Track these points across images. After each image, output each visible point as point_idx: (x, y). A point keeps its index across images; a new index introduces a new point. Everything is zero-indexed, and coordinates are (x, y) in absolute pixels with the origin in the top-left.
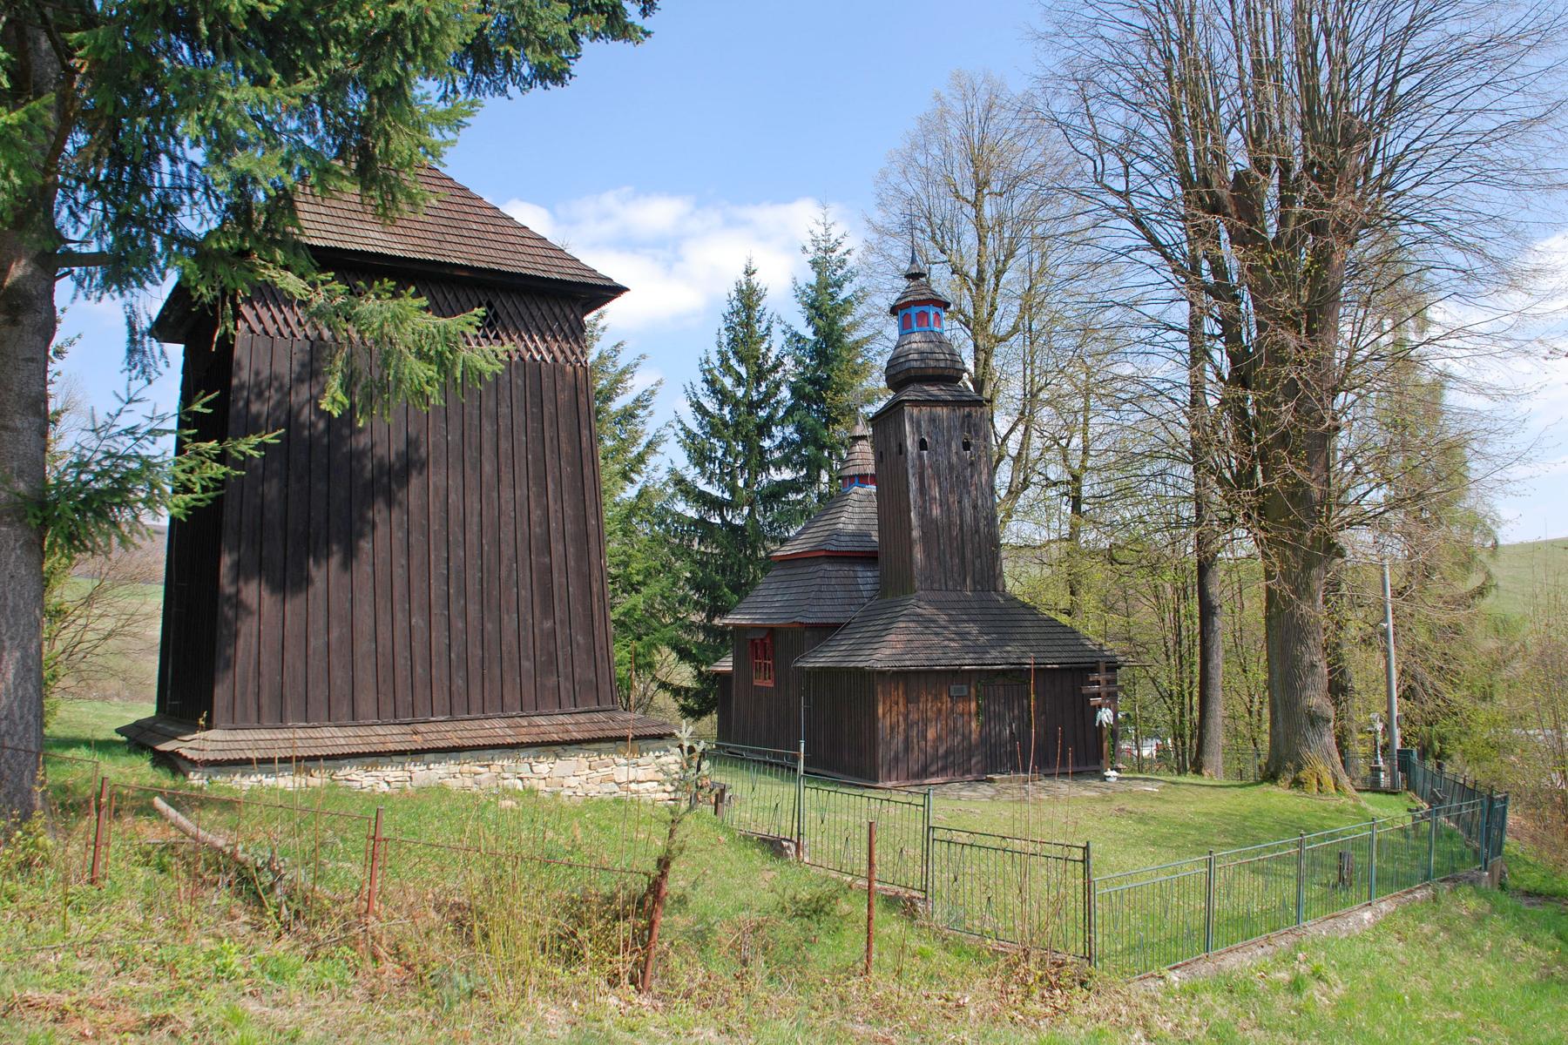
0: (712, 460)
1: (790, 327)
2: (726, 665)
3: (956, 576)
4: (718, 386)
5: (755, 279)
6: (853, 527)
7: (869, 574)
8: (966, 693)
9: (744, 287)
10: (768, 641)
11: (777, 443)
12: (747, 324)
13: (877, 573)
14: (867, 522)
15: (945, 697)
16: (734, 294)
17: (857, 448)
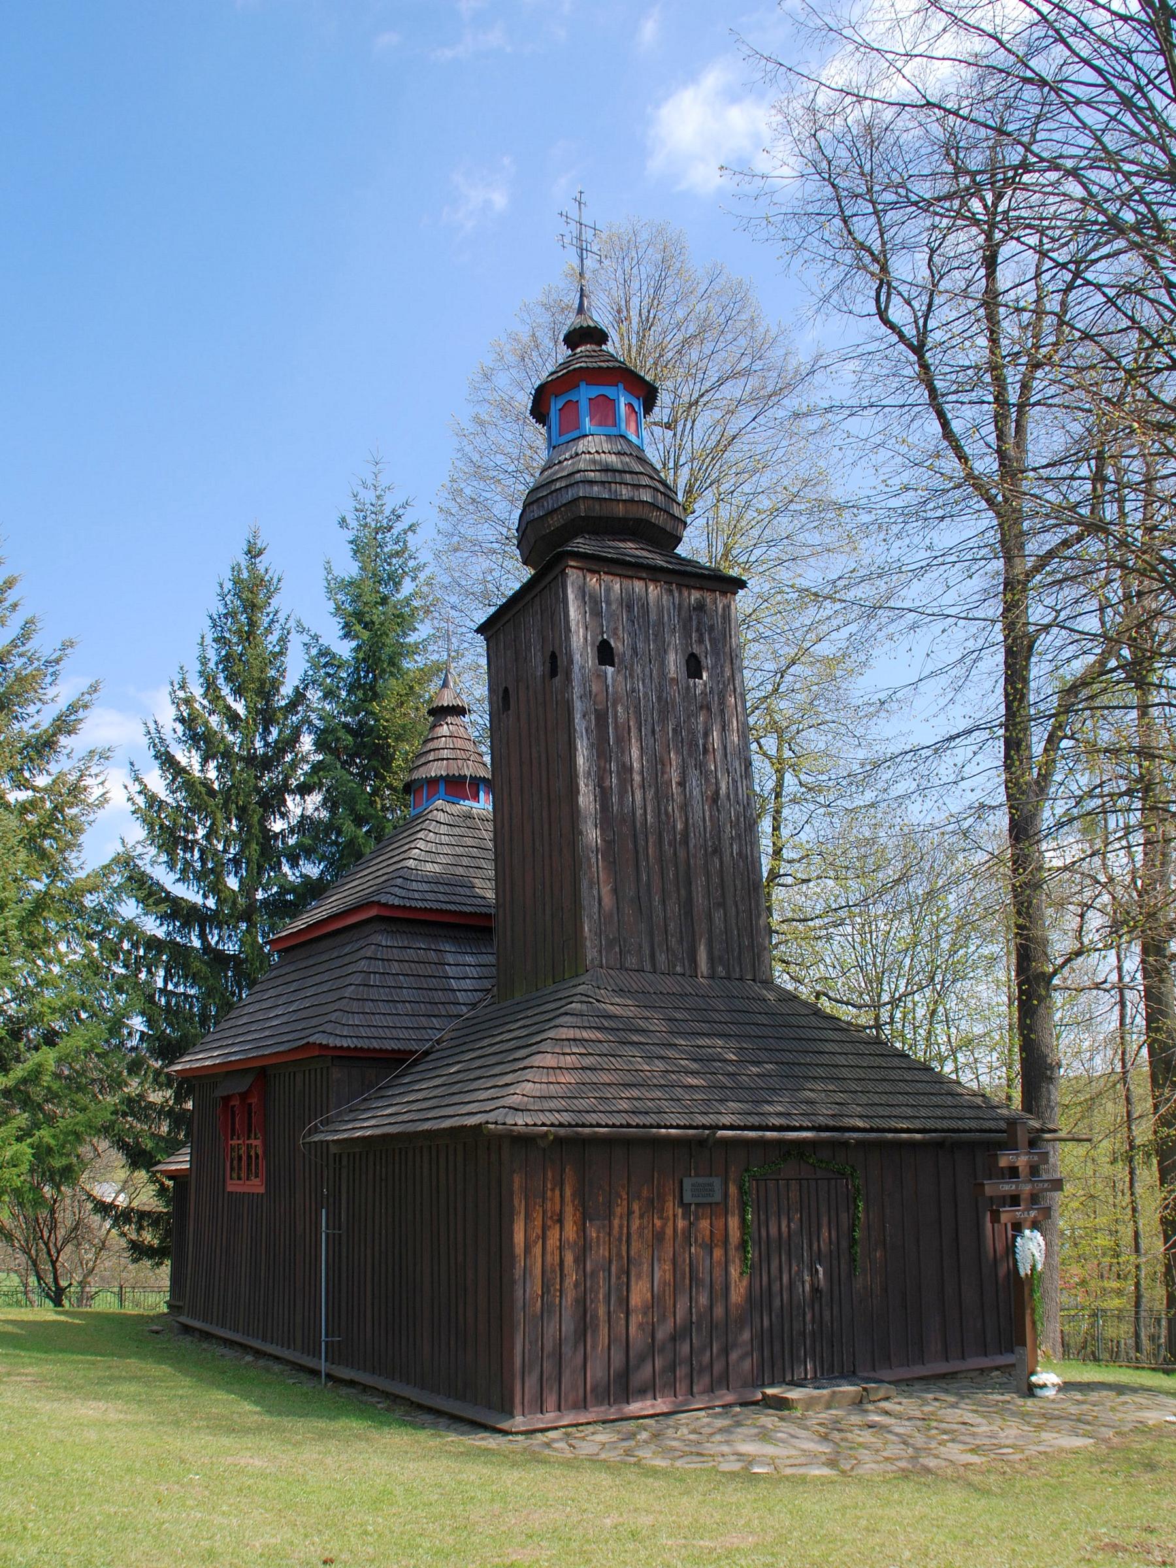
0: (188, 846)
1: (316, 638)
2: (181, 1161)
3: (673, 942)
4: (200, 730)
5: (262, 563)
6: (437, 868)
7: (469, 959)
8: (718, 1197)
9: (245, 575)
10: (254, 1100)
11: (294, 822)
12: (249, 635)
13: (491, 959)
14: (465, 861)
15: (671, 1206)
16: (228, 585)
17: (444, 730)
